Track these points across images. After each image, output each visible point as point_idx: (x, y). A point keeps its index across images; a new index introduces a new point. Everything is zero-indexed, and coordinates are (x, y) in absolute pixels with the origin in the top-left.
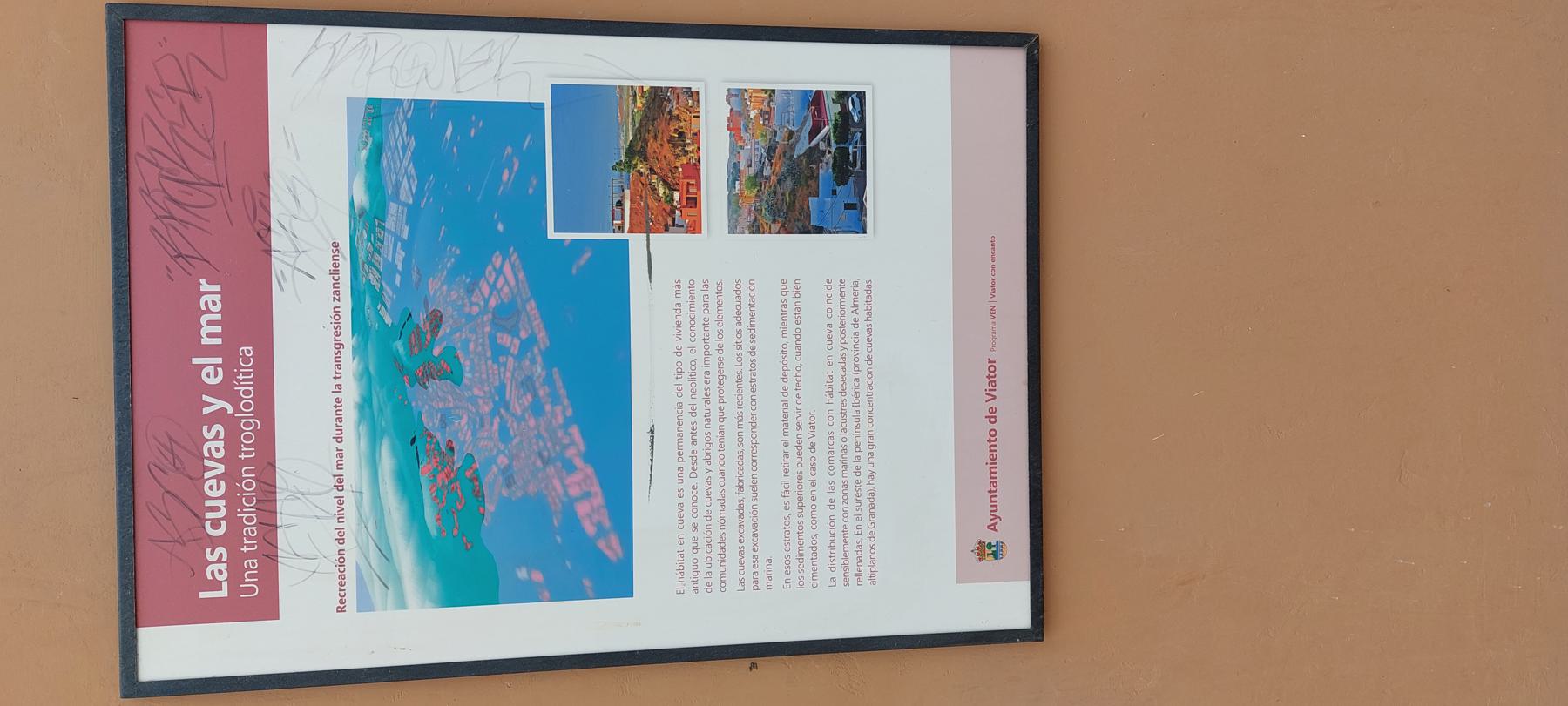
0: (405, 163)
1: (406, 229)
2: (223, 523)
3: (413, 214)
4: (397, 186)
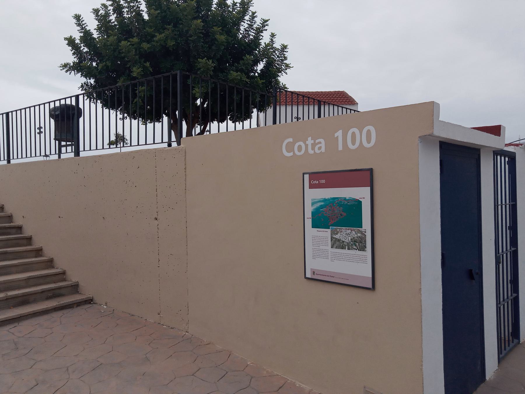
2: (291, 154)
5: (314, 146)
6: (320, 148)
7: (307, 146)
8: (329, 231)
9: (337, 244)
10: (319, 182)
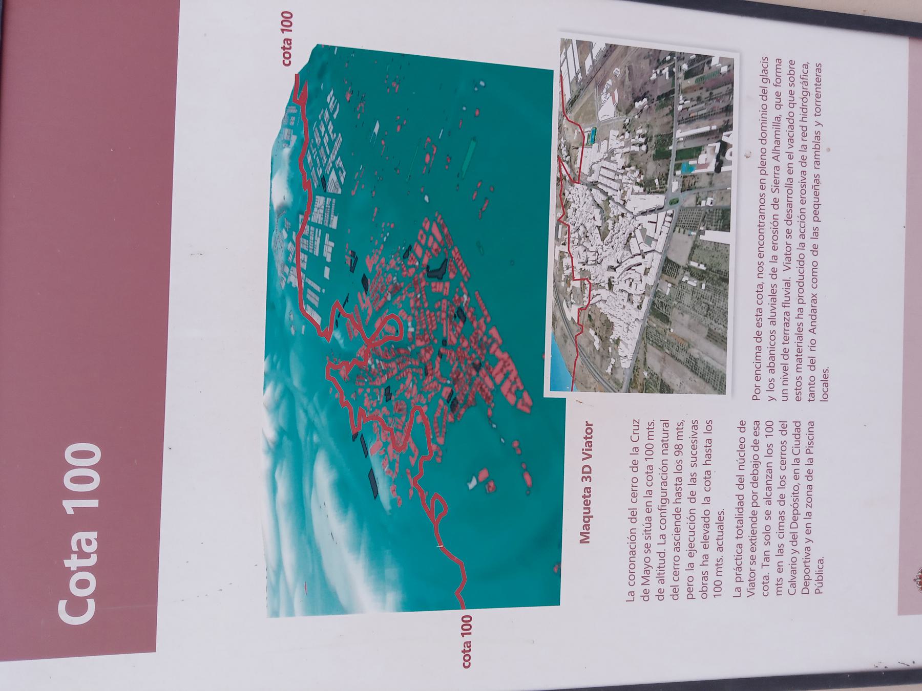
0: (332, 157)
1: (335, 220)
2: (91, 603)
3: (342, 204)
4: (324, 181)
5: (83, 555)
6: (89, 542)
7: (80, 569)
8: (583, 409)
9: (684, 332)
10: (83, 519)
